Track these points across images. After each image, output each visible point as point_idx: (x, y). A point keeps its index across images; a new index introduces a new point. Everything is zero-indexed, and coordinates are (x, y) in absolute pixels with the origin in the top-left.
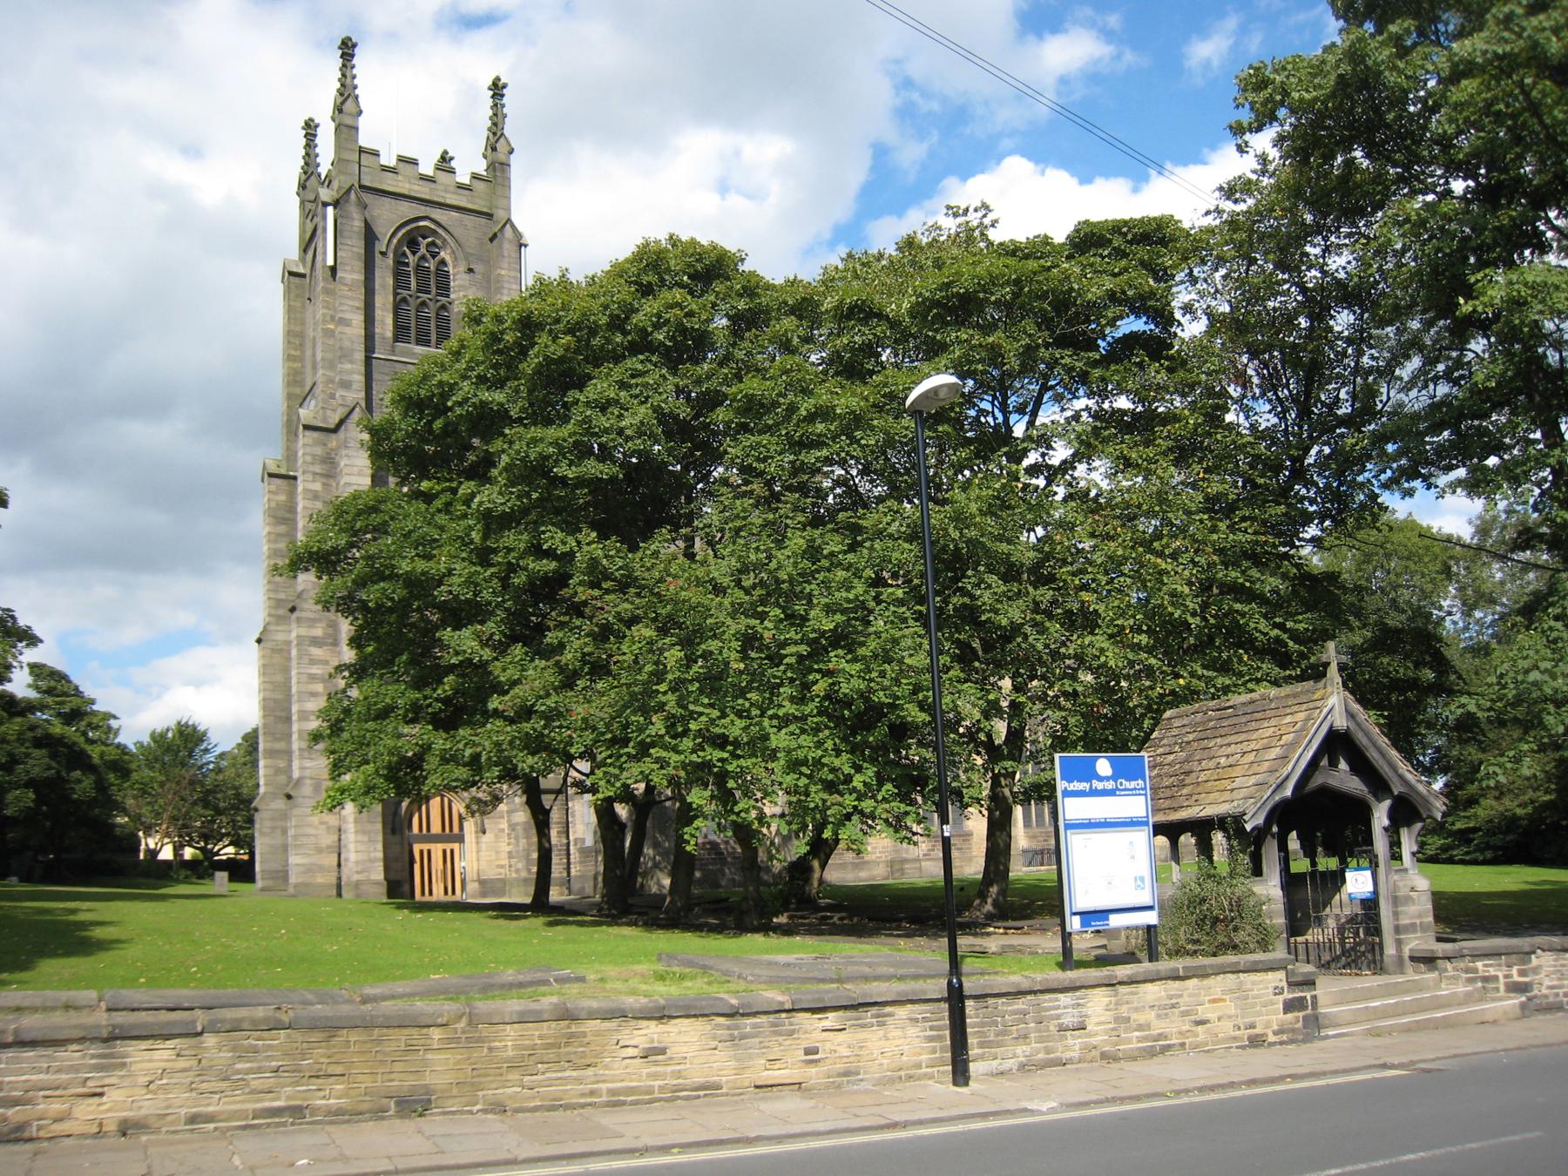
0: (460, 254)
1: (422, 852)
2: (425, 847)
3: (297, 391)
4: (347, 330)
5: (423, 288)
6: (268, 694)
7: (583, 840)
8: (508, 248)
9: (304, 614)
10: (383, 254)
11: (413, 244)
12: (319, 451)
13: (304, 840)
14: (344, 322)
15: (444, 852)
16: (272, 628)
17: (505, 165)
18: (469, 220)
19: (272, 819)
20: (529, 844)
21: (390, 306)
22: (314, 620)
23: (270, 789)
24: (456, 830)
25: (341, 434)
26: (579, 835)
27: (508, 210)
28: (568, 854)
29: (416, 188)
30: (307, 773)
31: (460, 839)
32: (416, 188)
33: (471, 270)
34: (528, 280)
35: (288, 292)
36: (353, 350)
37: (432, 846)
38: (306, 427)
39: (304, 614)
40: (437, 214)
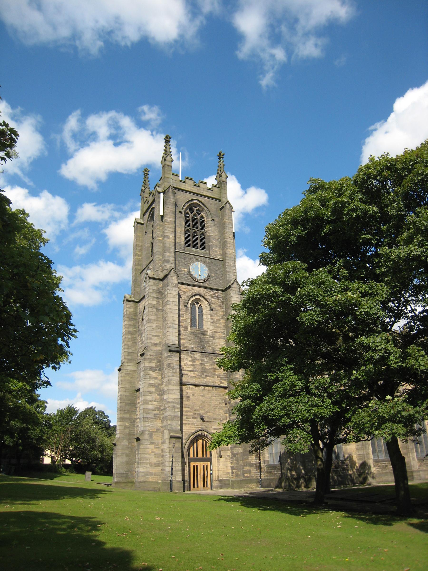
0: (209, 213)
1: (194, 466)
2: (195, 464)
3: (139, 268)
4: (168, 240)
5: (195, 226)
6: (123, 393)
7: (268, 461)
8: (227, 212)
9: (148, 357)
10: (180, 212)
11: (191, 210)
12: (155, 288)
13: (144, 460)
14: (168, 237)
15: (204, 466)
16: (126, 364)
17: (225, 182)
18: (212, 201)
19: (122, 449)
20: (132, 454)
21: (183, 232)
22: (152, 359)
23: (122, 436)
24: (208, 456)
25: (165, 281)
26: (266, 459)
27: (226, 198)
28: (260, 468)
29: (192, 189)
30: (147, 428)
31: (210, 460)
32: (192, 189)
33: (213, 220)
34: (365, 161)
35: (136, 231)
36: (170, 248)
37: (198, 464)
38: (150, 278)
39: (148, 357)
40: (200, 199)
